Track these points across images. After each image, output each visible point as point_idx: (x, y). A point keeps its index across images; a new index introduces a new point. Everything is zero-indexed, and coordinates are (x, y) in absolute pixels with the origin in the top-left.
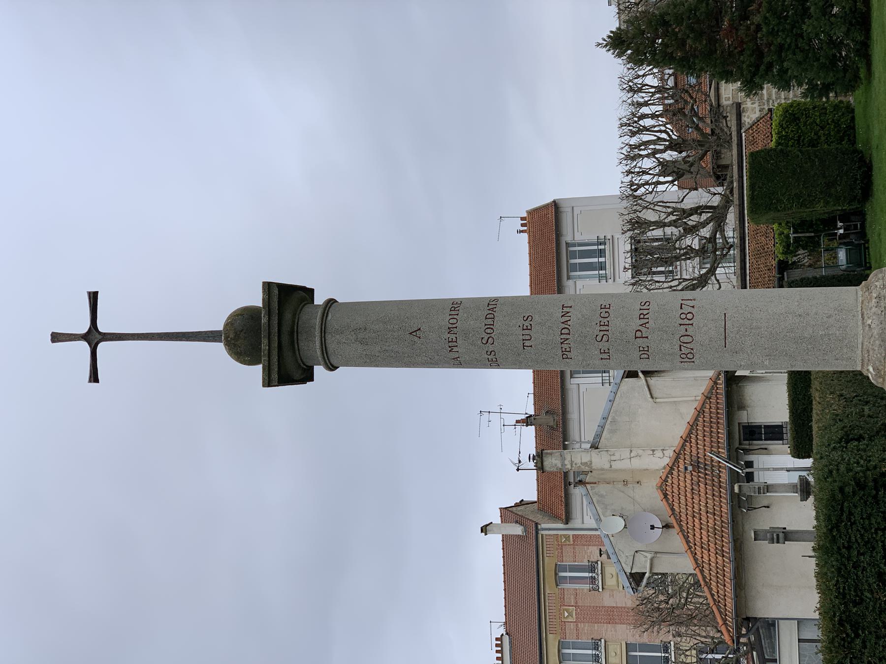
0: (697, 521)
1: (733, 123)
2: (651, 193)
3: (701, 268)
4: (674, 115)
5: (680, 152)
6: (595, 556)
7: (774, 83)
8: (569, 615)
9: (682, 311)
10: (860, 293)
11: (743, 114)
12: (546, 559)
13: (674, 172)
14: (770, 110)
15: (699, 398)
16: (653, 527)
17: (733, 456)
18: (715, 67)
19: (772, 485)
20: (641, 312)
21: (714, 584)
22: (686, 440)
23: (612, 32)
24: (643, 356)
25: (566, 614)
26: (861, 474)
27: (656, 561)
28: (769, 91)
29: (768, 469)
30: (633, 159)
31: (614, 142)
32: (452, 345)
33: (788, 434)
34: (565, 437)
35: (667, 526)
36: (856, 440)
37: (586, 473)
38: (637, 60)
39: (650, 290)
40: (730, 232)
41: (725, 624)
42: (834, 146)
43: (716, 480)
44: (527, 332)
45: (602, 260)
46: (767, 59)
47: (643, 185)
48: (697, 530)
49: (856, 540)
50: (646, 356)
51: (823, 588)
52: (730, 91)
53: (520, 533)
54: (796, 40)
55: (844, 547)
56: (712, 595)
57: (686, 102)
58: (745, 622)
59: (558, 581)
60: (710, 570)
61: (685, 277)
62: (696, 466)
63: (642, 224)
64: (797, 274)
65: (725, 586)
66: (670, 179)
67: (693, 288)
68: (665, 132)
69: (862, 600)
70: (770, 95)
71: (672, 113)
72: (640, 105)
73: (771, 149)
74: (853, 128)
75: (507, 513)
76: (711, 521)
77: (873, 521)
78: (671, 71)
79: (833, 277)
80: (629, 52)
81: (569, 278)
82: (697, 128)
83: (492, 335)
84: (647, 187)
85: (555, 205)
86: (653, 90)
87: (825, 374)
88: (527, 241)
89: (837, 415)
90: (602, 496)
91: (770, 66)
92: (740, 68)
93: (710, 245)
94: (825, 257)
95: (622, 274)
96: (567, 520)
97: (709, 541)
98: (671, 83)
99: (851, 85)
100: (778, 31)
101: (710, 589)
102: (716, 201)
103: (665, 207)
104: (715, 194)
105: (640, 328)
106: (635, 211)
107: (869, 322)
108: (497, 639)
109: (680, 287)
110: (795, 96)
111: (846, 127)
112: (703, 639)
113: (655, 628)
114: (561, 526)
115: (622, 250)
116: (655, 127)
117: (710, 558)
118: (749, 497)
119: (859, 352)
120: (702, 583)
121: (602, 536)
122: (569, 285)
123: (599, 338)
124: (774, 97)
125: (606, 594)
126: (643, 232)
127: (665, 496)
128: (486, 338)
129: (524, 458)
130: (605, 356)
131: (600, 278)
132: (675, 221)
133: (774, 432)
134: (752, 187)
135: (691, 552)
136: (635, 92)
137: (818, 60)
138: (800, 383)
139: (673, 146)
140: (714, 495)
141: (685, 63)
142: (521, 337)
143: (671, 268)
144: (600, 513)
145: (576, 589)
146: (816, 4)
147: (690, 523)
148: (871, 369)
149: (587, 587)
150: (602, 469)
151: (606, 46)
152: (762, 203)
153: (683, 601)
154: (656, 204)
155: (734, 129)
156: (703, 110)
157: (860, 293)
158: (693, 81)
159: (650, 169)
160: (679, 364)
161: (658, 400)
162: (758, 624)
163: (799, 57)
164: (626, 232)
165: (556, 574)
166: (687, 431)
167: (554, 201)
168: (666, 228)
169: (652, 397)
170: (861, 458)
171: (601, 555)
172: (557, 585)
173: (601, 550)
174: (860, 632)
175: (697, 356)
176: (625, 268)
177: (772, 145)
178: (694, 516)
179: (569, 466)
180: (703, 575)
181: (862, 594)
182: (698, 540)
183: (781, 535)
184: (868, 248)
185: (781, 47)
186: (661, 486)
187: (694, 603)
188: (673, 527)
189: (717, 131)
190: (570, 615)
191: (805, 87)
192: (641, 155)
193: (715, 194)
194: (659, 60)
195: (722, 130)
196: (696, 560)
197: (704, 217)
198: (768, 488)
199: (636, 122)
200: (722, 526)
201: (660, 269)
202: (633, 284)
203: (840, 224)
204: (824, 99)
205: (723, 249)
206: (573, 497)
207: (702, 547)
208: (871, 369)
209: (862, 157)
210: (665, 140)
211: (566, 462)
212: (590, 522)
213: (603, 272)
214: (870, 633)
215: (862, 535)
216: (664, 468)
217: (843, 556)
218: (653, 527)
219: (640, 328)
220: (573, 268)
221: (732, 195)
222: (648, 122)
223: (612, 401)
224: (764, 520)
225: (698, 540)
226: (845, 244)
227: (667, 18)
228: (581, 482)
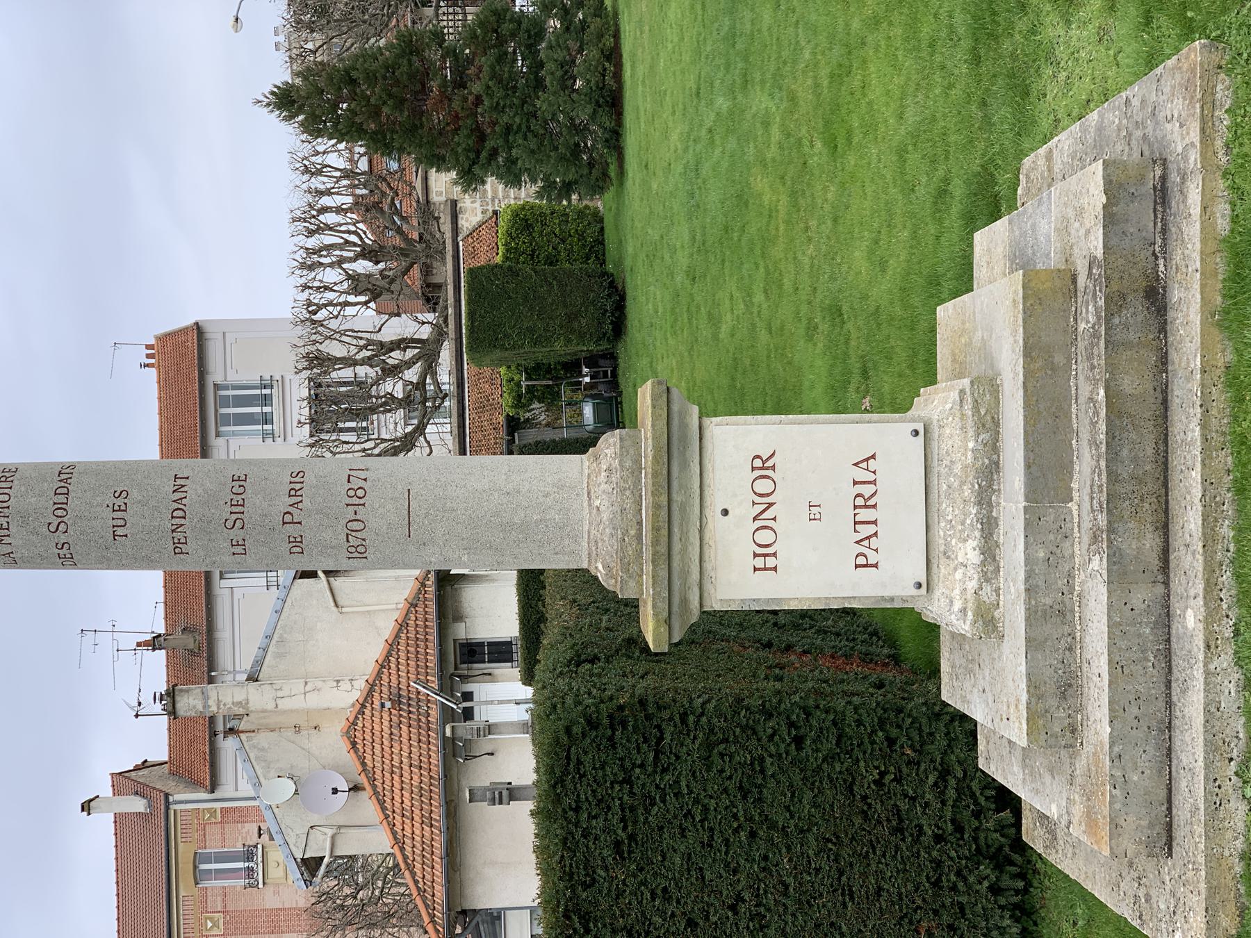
0: (396, 778)
1: (447, 228)
2: (336, 317)
3: (406, 424)
4: (367, 210)
5: (377, 263)
6: (253, 839)
7: (500, 177)
9: (350, 486)
10: (586, 464)
12: (181, 846)
13: (368, 289)
14: (495, 213)
15: (401, 606)
16: (335, 791)
17: (447, 686)
18: (421, 146)
19: (496, 725)
20: (293, 486)
21: (418, 866)
22: (383, 665)
23: (276, 86)
24: (294, 550)
25: (210, 924)
26: (593, 708)
27: (339, 841)
28: (492, 185)
30: (311, 268)
31: (283, 244)
33: (518, 655)
34: (212, 666)
35: (355, 788)
36: (590, 662)
37: (239, 717)
38: (313, 128)
39: (335, 454)
40: (445, 376)
41: (433, 921)
42: (577, 266)
44: (119, 514)
45: (267, 409)
46: (490, 144)
47: (325, 306)
48: (397, 791)
49: (587, 799)
50: (298, 550)
51: (545, 871)
52: (442, 183)
53: (142, 810)
54: (528, 121)
55: (571, 809)
56: (416, 882)
57: (383, 194)
58: (461, 917)
59: (198, 876)
60: (414, 846)
61: (384, 436)
62: (397, 701)
63: (324, 361)
64: (531, 436)
65: (433, 868)
66: (362, 299)
67: (395, 452)
69: (594, 880)
70: (495, 191)
71: (367, 208)
72: (320, 193)
74: (602, 243)
75: (124, 782)
76: (416, 777)
77: (608, 771)
78: (362, 150)
79: (577, 441)
80: (301, 117)
81: (218, 435)
82: (399, 230)
83: (65, 519)
85: (198, 329)
86: (338, 174)
87: (558, 573)
88: (155, 379)
89: (567, 628)
90: (263, 749)
91: (494, 153)
93: (418, 393)
94: (567, 413)
95: (297, 431)
98: (363, 165)
99: (599, 186)
100: (504, 107)
101: (413, 874)
102: (425, 333)
103: (356, 338)
104: (424, 323)
105: (290, 509)
106: (315, 342)
107: (597, 503)
109: (376, 451)
110: (528, 195)
111: (593, 241)
114: (204, 795)
115: (296, 397)
116: (341, 225)
117: (415, 830)
118: (468, 743)
119: (585, 544)
120: (402, 865)
121: (263, 808)
122: (218, 444)
123: (229, 524)
124: (500, 195)
125: (269, 890)
126: (325, 372)
127: (354, 744)
129: (147, 698)
130: (239, 550)
131: (264, 435)
132: (369, 358)
133: (500, 652)
134: (471, 314)
137: (556, 148)
138: (532, 585)
139: (367, 253)
140: (420, 741)
141: (380, 143)
142: (111, 523)
143: (364, 424)
145: (224, 888)
146: (552, 74)
147: (388, 782)
148: (600, 567)
149: (242, 882)
150: (264, 711)
151: (268, 105)
152: (484, 338)
153: (377, 892)
154: (343, 333)
155: (448, 235)
156: (407, 206)
157: (586, 464)
158: (394, 166)
159: (335, 284)
160: (346, 561)
161: (344, 610)
162: (478, 918)
163: (533, 144)
165: (195, 867)
166: (385, 653)
167: (197, 324)
168: (358, 367)
169: (337, 605)
170: (594, 686)
171: (260, 835)
172: (197, 883)
173: (260, 829)
174: (591, 925)
175: (370, 550)
176: (300, 422)
177: (499, 259)
178: (393, 772)
179: (214, 709)
180: (403, 855)
181: (594, 872)
182: (397, 805)
183: (505, 793)
184: (621, 403)
185: (508, 129)
186: (348, 732)
187: (394, 895)
188: (364, 789)
189: (427, 236)
191: (540, 184)
192: (321, 264)
193: (424, 323)
194: (347, 131)
196: (394, 834)
197: (410, 353)
198: (490, 728)
201: (348, 424)
202: (311, 446)
203: (585, 370)
204: (565, 202)
205: (435, 399)
206: (223, 753)
208: (600, 567)
209: (613, 282)
210: (355, 245)
211: (211, 702)
212: (246, 789)
213: (268, 427)
214: (605, 926)
215: (593, 791)
216: (353, 705)
217: (570, 822)
218: (335, 791)
220: (225, 420)
222: (330, 218)
223: (279, 612)
224: (485, 773)
225: (397, 805)
226: (593, 397)
227: (354, 74)
228: (231, 731)
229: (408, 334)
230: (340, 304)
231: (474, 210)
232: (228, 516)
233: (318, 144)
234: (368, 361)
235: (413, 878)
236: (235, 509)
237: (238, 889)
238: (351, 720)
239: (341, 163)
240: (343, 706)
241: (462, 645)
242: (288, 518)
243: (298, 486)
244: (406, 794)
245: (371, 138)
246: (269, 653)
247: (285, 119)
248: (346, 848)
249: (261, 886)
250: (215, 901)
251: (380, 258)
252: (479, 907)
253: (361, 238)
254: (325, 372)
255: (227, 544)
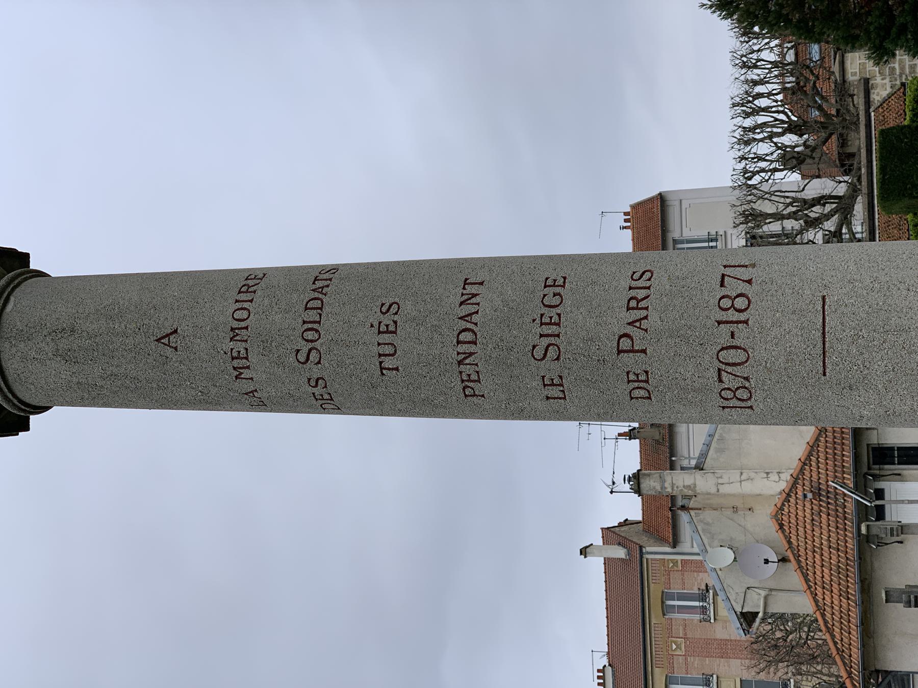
0: (817, 556)
1: (860, 100)
5: (801, 136)
8: (678, 648)
9: (724, 291)
11: (872, 91)
12: (652, 586)
14: (903, 85)
16: (767, 561)
17: (860, 486)
20: (633, 293)
22: (805, 463)
24: (636, 393)
25: (674, 647)
27: (771, 600)
29: (902, 502)
30: (747, 143)
31: (726, 124)
32: (239, 364)
34: (672, 452)
35: (783, 560)
37: (689, 498)
43: (840, 510)
44: (386, 338)
47: (758, 172)
50: (642, 393)
52: (858, 63)
53: (623, 557)
57: (807, 80)
59: (665, 610)
60: (833, 614)
62: (817, 493)
63: (757, 216)
65: (850, 633)
68: (783, 112)
71: (793, 94)
72: (755, 83)
73: (905, 126)
75: (610, 534)
83: (317, 344)
84: (763, 174)
85: (661, 199)
86: (770, 66)
90: (708, 524)
92: (867, 32)
96: (675, 543)
97: (832, 580)
98: (790, 57)
102: (841, 190)
103: (784, 197)
104: (840, 182)
105: (629, 330)
108: (599, 671)
112: (825, 678)
113: (772, 669)
117: (832, 599)
123: (538, 353)
125: (718, 627)
127: (781, 526)
128: (305, 350)
129: (619, 479)
130: (555, 392)
132: (794, 213)
134: (883, 169)
135: (812, 593)
136: (749, 68)
139: (792, 128)
140: (837, 528)
142: (376, 350)
144: (706, 542)
147: (810, 559)
149: (697, 617)
150: (709, 494)
151: (711, 7)
154: (772, 194)
155: (862, 108)
156: (826, 88)
159: (767, 155)
160: (719, 411)
162: (889, 678)
164: (738, 225)
165: (663, 602)
166: (807, 453)
167: (660, 194)
168: (785, 221)
172: (664, 615)
175: (758, 395)
178: (814, 551)
179: (669, 490)
186: (776, 515)
188: (790, 561)
190: (678, 647)
192: (755, 140)
193: (840, 182)
195: (848, 111)
196: (816, 601)
197: (828, 208)
198: (903, 529)
199: (749, 102)
200: (847, 564)
207: (824, 588)
210: (783, 122)
211: (667, 485)
216: (780, 493)
218: (767, 561)
219: (629, 330)
221: (860, 184)
229: (826, 192)
230: (770, 170)
231: (884, 85)
232: (536, 340)
233: (754, 44)
234: (793, 216)
235: (833, 640)
236: (546, 330)
237: (695, 622)
238: (779, 506)
239: (772, 57)
240: (772, 493)
241: (874, 449)
242: (625, 344)
243: (641, 294)
244: (826, 571)
245: (795, 26)
246: (712, 448)
247: (725, 18)
248: (777, 607)
249: (712, 621)
250: (678, 629)
251: (804, 131)
252: (891, 668)
253: (788, 117)
254: (758, 226)
255: (537, 383)
